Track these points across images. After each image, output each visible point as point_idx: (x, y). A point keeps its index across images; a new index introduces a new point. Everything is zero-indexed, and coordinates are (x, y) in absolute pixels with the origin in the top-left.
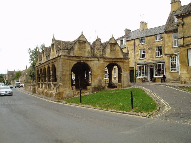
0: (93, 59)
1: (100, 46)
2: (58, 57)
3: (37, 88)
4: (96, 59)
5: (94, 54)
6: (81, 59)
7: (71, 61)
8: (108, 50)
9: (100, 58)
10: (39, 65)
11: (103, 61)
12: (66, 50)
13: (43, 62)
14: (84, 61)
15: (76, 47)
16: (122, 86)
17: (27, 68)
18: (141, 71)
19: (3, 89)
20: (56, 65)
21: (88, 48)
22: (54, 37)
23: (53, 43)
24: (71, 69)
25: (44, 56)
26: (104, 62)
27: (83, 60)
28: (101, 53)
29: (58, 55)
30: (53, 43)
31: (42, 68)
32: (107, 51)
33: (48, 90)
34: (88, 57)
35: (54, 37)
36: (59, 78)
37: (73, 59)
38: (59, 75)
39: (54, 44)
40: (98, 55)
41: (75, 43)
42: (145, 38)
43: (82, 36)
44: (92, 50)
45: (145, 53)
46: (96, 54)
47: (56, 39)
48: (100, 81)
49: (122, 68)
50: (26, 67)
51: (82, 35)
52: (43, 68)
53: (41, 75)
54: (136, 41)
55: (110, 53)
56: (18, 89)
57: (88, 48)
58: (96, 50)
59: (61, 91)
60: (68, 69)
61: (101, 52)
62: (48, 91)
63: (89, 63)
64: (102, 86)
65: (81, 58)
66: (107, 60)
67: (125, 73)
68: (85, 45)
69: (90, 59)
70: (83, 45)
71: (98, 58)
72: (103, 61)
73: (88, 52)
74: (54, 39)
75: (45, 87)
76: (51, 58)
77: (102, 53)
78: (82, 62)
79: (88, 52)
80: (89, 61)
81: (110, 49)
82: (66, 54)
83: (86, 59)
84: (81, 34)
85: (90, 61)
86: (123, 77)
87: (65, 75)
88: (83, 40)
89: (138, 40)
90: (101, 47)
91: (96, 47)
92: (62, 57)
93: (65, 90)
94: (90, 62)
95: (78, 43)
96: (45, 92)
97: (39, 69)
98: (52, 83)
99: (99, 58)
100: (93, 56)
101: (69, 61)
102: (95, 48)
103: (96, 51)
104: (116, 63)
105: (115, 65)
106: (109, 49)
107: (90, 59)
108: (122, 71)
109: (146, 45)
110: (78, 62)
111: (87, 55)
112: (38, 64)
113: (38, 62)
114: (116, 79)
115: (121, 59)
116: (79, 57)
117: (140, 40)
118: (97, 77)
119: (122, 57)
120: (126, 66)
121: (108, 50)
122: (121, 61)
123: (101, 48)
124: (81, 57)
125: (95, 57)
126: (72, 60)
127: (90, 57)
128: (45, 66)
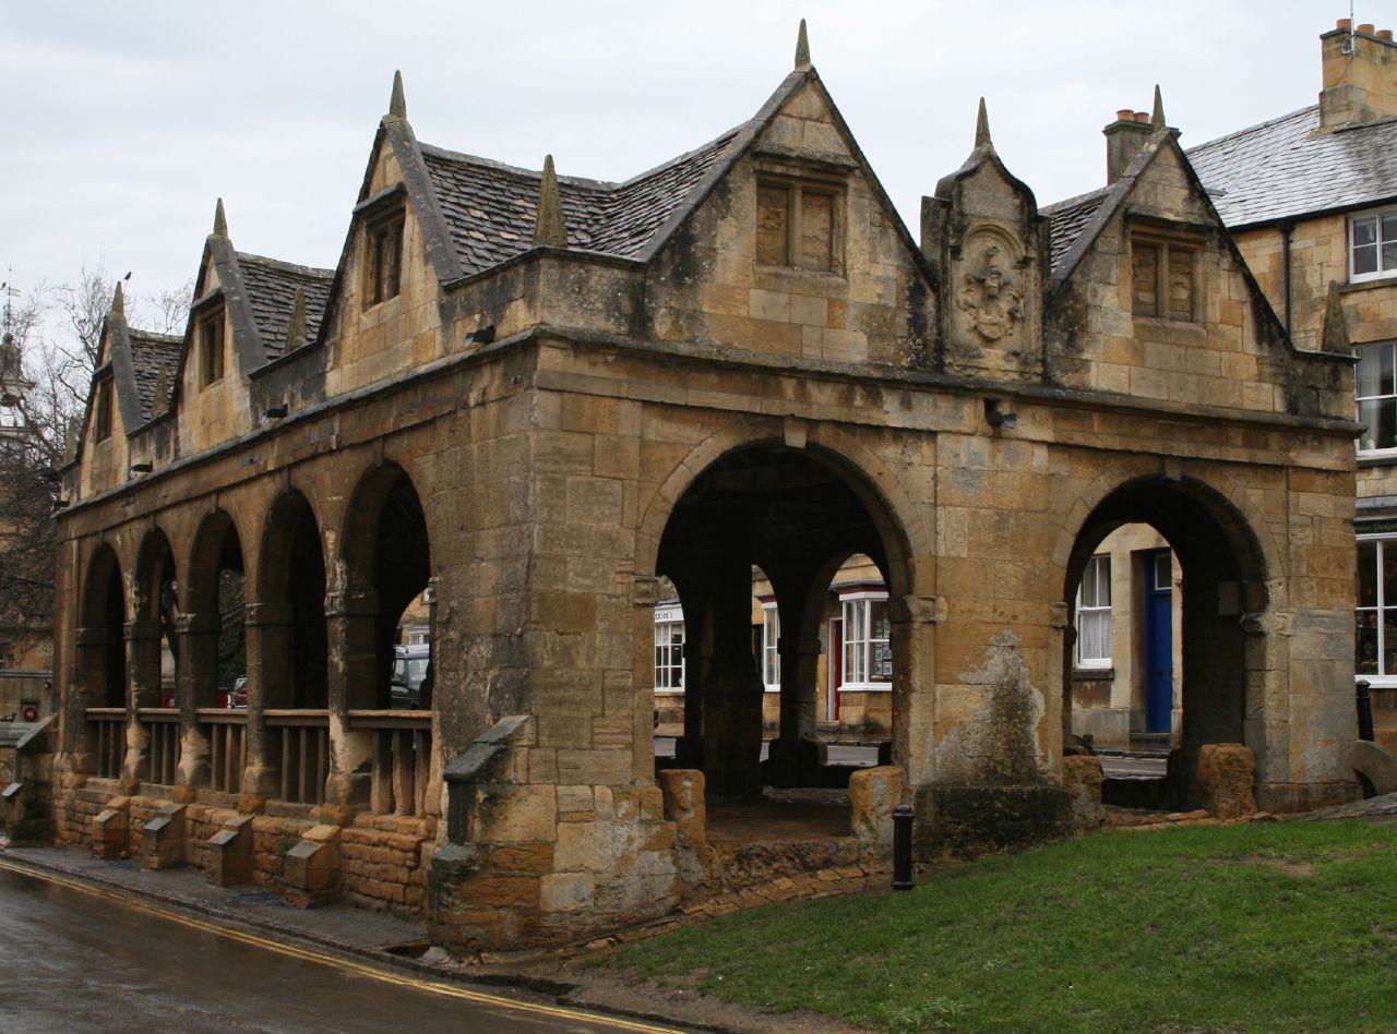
0: (927, 412)
3: (70, 777)
4: (971, 414)
6: (785, 401)
7: (657, 428)
9: (1023, 400)
11: (1051, 446)
12: (597, 270)
13: (193, 439)
14: (824, 437)
18: (1380, 607)
19: (2, 680)
20: (428, 470)
22: (398, 105)
24: (658, 523)
25: (212, 372)
26: (1062, 467)
27: (812, 424)
28: (1028, 336)
30: (214, 282)
31: (171, 521)
32: (1096, 322)
33: (260, 810)
34: (871, 386)
35: (398, 105)
36: (482, 650)
37: (695, 397)
38: (479, 601)
40: (996, 365)
41: (720, 188)
43: (809, 102)
44: (915, 295)
47: (246, 241)
48: (1010, 705)
49: (1271, 550)
51: (805, 80)
52: (181, 526)
53: (144, 610)
54: (1302, 241)
55: (1137, 352)
58: (962, 294)
61: (1034, 325)
62: (260, 822)
63: (880, 462)
64: (1033, 775)
65: (789, 386)
66: (1101, 435)
67: (1307, 619)
68: (835, 228)
69: (892, 413)
70: (809, 224)
71: (990, 406)
72: (1051, 446)
73: (876, 323)
75: (218, 771)
76: (339, 382)
77: (1046, 341)
78: (796, 439)
80: (878, 431)
81: (1136, 302)
82: (602, 324)
83: (847, 400)
84: (788, 66)
85: (898, 433)
87: (582, 612)
89: (1334, 230)
91: (973, 252)
92: (549, 359)
94: (891, 451)
95: (746, 194)
96: (222, 837)
97: (127, 543)
98: (336, 727)
99: (1004, 409)
101: (629, 419)
102: (961, 270)
104: (1213, 481)
105: (235, 682)
106: (1127, 290)
107: (892, 413)
108: (1276, 590)
110: (762, 434)
111: (853, 349)
112: (96, 478)
113: (106, 456)
114: (1105, 696)
115: (1256, 428)
116: (765, 376)
118: (980, 659)
119: (1266, 399)
120: (1314, 521)
122: (1262, 457)
123: (1033, 271)
124: (793, 372)
125: (960, 391)
126: (668, 409)
127: (893, 384)
128: (230, 501)
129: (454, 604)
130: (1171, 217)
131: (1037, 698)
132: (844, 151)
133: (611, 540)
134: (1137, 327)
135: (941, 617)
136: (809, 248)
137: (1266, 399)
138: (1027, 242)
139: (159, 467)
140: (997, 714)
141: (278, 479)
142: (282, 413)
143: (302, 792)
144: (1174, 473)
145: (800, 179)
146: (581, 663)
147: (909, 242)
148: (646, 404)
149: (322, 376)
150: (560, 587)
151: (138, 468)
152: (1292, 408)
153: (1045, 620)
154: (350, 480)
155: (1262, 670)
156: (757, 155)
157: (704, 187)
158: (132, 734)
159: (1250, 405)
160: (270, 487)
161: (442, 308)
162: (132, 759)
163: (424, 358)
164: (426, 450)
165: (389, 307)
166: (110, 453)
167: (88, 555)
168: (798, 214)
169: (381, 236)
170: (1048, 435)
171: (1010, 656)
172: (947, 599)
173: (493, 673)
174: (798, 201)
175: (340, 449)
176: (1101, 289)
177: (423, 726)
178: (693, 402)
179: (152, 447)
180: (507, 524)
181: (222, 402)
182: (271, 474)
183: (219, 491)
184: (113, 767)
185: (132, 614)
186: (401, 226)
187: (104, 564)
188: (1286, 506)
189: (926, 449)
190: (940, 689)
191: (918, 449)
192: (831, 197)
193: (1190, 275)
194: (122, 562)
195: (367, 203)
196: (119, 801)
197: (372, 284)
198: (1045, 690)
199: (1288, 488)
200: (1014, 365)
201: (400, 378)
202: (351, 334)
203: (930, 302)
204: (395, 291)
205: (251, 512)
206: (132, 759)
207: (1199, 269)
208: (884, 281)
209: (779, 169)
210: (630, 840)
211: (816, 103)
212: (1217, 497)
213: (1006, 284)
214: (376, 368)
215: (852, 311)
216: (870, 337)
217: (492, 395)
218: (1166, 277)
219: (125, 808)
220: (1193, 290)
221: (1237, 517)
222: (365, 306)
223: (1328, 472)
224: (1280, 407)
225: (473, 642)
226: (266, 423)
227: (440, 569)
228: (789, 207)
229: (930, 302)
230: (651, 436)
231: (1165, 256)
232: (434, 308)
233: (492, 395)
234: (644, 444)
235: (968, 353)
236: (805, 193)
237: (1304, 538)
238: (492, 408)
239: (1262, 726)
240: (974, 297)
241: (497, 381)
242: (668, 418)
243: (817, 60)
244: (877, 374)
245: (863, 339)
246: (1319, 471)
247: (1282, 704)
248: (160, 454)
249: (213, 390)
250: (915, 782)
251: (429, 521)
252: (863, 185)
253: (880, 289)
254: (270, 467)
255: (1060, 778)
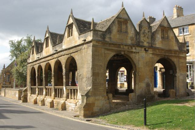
0: (138, 49)
1: (148, 30)
2: (83, 44)
5: (139, 42)
7: (106, 52)
8: (159, 36)
10: (36, 61)
14: (126, 53)
15: (115, 29)
16: (177, 94)
17: (5, 67)
21: (132, 32)
23: (69, 23)
24: (106, 63)
25: (47, 46)
27: (124, 51)
28: (149, 40)
29: (85, 40)
30: (47, 35)
32: (157, 39)
36: (84, 79)
37: (110, 48)
38: (84, 73)
39: (48, 37)
40: (146, 44)
41: (113, 22)
42: (190, 27)
44: (136, 35)
45: (190, 48)
46: (143, 42)
49: (177, 66)
50: (4, 66)
52: (43, 65)
55: (162, 42)
56: (171, 121)
57: (132, 32)
59: (91, 102)
60: (101, 64)
61: (150, 39)
63: (132, 56)
65: (122, 46)
67: (181, 74)
68: (127, 27)
72: (152, 54)
73: (132, 39)
74: (48, 31)
77: (151, 41)
78: (123, 53)
79: (132, 39)
80: (132, 52)
81: (161, 37)
84: (121, 8)
85: (134, 52)
86: (179, 81)
88: (126, 17)
90: (149, 32)
93: (98, 100)
94: (134, 54)
97: (36, 67)
100: (138, 44)
101: (103, 51)
103: (142, 39)
104: (171, 58)
106: (160, 35)
108: (178, 71)
109: (190, 36)
111: (129, 42)
112: (32, 59)
115: (176, 51)
116: (119, 45)
117: (180, 30)
119: (176, 48)
121: (159, 36)
123: (150, 33)
126: (108, 50)
129: (81, 73)
130: (165, 26)
131: (151, 84)
132: (128, 18)
133: (101, 65)
134: (162, 40)
135: (140, 75)
136: (124, 30)
137: (176, 48)
138: (149, 29)
139: (40, 58)
140: (146, 86)
141: (56, 59)
142: (57, 51)
143: (60, 96)
144: (166, 57)
145: (123, 21)
146: (98, 81)
147: (136, 31)
148: (105, 49)
149: (62, 46)
150: (95, 71)
151: (38, 58)
152: (179, 49)
153: (152, 75)
154: (66, 59)
155: (176, 80)
156: (118, 18)
157: (111, 22)
158: (37, 89)
159: (175, 49)
160: (55, 60)
161: (78, 37)
162: (37, 92)
163: (76, 43)
164: (76, 55)
165: (71, 37)
166: (34, 56)
167: (31, 68)
168: (122, 26)
169: (70, 29)
170: (152, 52)
171: (148, 79)
172: (141, 72)
173: (86, 82)
174: (122, 24)
175: (65, 55)
176: (158, 35)
177: (77, 88)
178: (110, 48)
179: (39, 55)
180: (88, 64)
181: (49, 49)
182: (55, 58)
183: (48, 60)
184: (35, 93)
185: (37, 75)
186: (72, 28)
187: (33, 70)
188: (179, 61)
189: (138, 54)
190: (140, 83)
191: (137, 54)
192: (126, 23)
193: (168, 33)
194: (36, 69)
195: (68, 25)
196: (36, 97)
197: (68, 35)
198: (152, 83)
199: (179, 59)
200: (148, 44)
201: (73, 46)
202: (66, 41)
203: (138, 36)
204: (72, 35)
205: (52, 63)
206: (37, 92)
207: (168, 33)
208: (133, 34)
209: (120, 20)
210: (104, 102)
211: (125, 12)
212: (171, 60)
213: (147, 34)
214: (69, 45)
215: (129, 37)
216: (131, 41)
217: (86, 48)
218: (165, 34)
219: (36, 98)
220: (168, 35)
221: (173, 62)
222: (68, 37)
223: (183, 57)
224: (178, 49)
225: (83, 78)
226: (55, 52)
227: (79, 69)
228: (121, 25)
229: (138, 36)
230: (106, 53)
231: (165, 31)
232: (78, 37)
233: (86, 48)
234: (105, 53)
235: (143, 42)
236: (123, 23)
237: (181, 65)
238: (86, 49)
239: (176, 87)
240: (143, 35)
241: (86, 46)
242: (107, 51)
243: (124, 7)
244: (132, 45)
245: (130, 41)
246: (183, 57)
247: (179, 84)
248: (40, 56)
249: (47, 48)
250: (137, 94)
251: (77, 63)
252: (130, 22)
253: (132, 35)
254: (55, 57)
255: (154, 94)
